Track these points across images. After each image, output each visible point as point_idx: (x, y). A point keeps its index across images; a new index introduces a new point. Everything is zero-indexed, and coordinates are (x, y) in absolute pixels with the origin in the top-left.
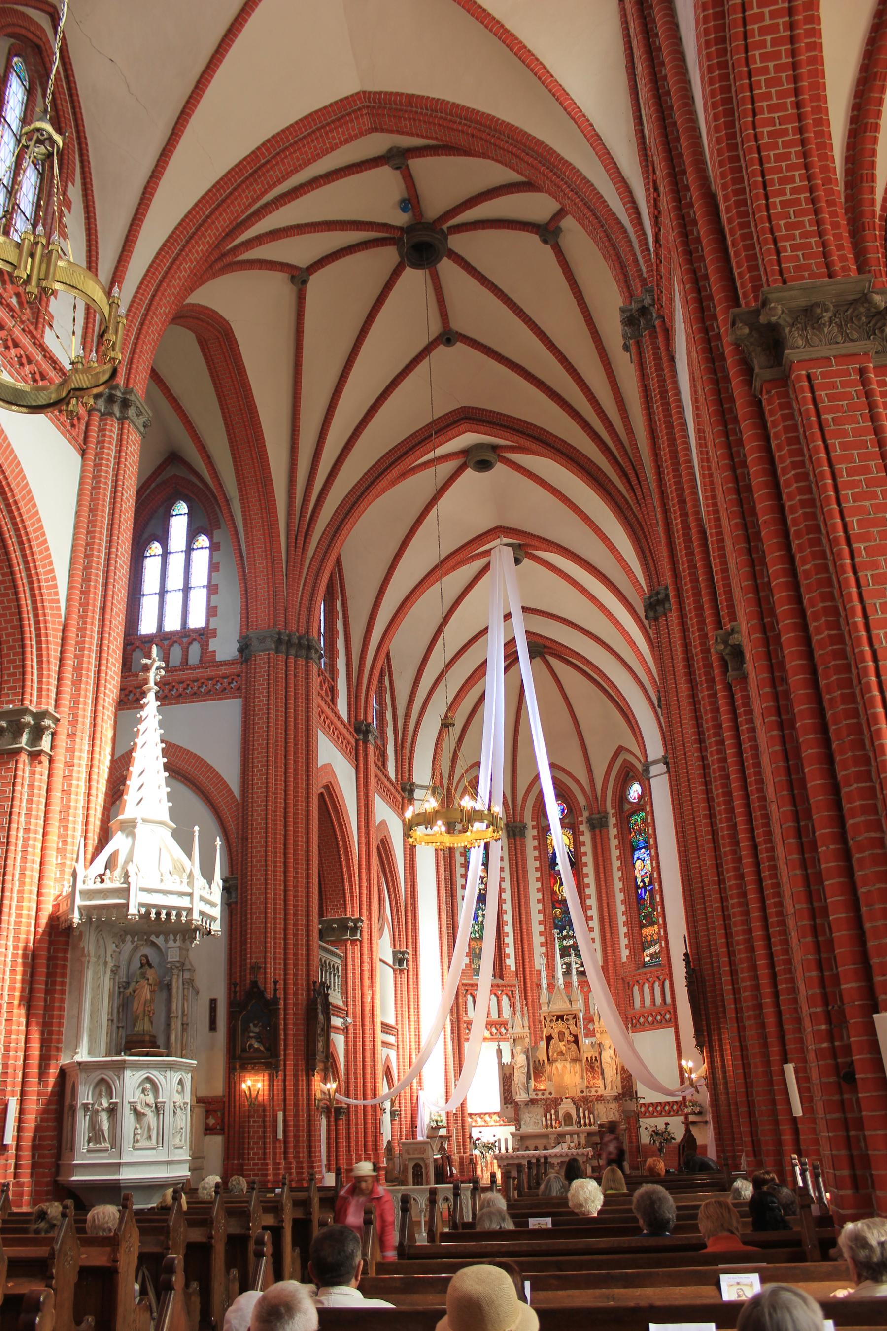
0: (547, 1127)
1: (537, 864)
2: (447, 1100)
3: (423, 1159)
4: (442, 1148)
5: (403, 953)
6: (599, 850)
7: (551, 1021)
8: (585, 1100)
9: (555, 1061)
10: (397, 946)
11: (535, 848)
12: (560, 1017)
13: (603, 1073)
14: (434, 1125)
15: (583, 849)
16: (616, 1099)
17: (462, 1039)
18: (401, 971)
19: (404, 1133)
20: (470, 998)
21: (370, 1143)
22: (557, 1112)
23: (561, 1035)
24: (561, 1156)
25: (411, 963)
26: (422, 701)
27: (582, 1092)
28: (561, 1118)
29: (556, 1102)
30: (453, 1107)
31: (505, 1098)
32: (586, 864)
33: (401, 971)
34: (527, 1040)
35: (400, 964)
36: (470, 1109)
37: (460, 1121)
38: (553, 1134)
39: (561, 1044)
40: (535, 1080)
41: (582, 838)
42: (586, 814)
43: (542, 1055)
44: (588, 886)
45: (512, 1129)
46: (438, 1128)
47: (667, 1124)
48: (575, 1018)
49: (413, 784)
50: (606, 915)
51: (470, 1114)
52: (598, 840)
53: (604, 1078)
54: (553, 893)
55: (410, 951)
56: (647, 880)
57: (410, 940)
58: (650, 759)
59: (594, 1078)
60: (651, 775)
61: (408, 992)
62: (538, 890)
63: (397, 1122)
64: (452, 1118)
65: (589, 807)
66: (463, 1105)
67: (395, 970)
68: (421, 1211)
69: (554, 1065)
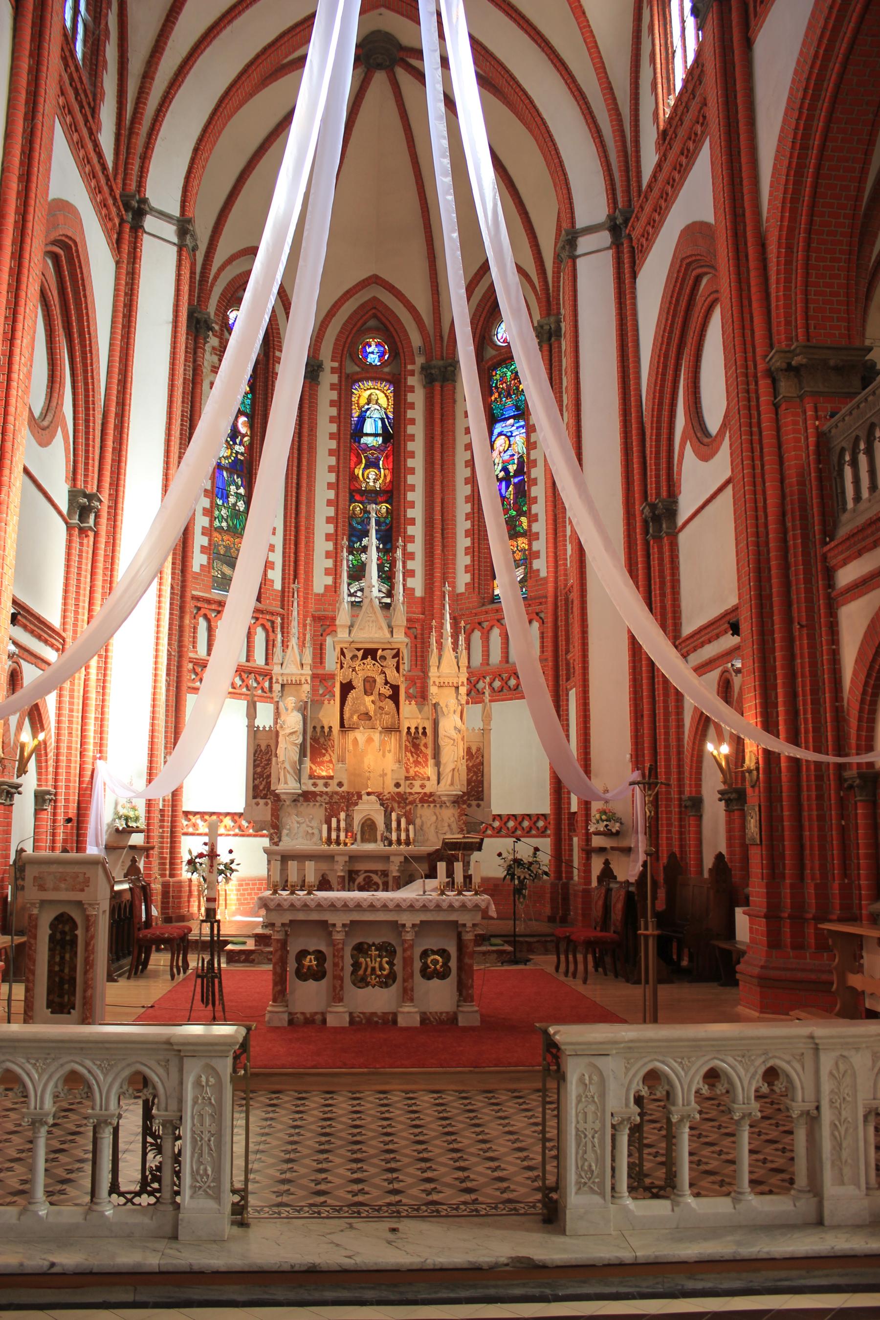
0: (329, 841)
1: (334, 428)
2: (150, 781)
3: (79, 904)
4: (132, 871)
5: (90, 497)
6: (437, 416)
7: (354, 657)
8: (402, 799)
9: (352, 728)
10: (80, 478)
11: (332, 403)
12: (370, 653)
13: (436, 755)
14: (121, 825)
15: (410, 414)
16: (458, 801)
17: (184, 688)
18: (82, 531)
19: (60, 838)
20: (202, 624)
21: (687, 769)
22: (349, 818)
23: (369, 684)
24: (424, 908)
25: (104, 521)
26: (178, 61)
27: (397, 785)
28: (356, 827)
29: (350, 800)
30: (161, 792)
31: (255, 788)
32: (412, 438)
33: (82, 531)
34: (307, 688)
35: (83, 517)
36: (188, 804)
37: (167, 824)
38: (342, 854)
39: (368, 699)
40: (313, 760)
41: (410, 398)
42: (420, 360)
43: (330, 715)
44: (412, 471)
45: (266, 842)
46: (129, 831)
47: (537, 849)
48: (397, 655)
49: (144, 201)
50: (438, 516)
51: (186, 814)
52: (437, 400)
53: (438, 764)
54: (354, 478)
55: (105, 497)
56: (512, 468)
57: (108, 467)
58: (579, 225)
59: (417, 763)
60: (579, 251)
61: (93, 574)
62: (331, 469)
63: (47, 816)
64: (156, 815)
65: (427, 350)
66: (176, 795)
67: (70, 528)
68: (36, 1123)
69: (351, 735)
